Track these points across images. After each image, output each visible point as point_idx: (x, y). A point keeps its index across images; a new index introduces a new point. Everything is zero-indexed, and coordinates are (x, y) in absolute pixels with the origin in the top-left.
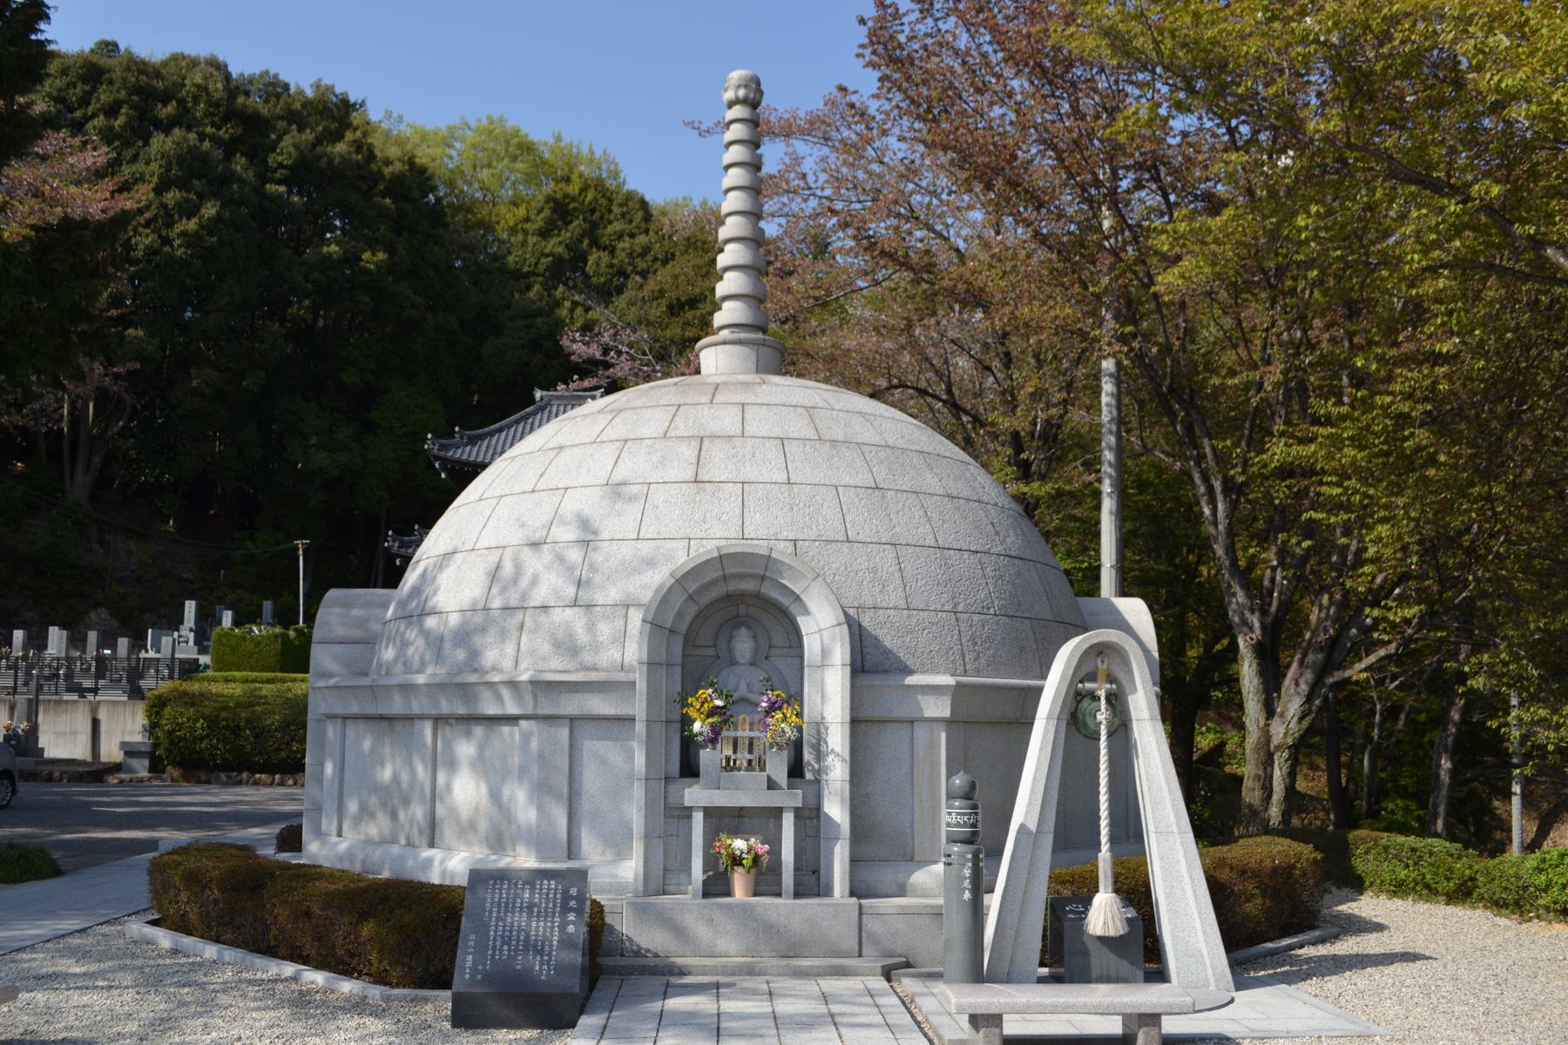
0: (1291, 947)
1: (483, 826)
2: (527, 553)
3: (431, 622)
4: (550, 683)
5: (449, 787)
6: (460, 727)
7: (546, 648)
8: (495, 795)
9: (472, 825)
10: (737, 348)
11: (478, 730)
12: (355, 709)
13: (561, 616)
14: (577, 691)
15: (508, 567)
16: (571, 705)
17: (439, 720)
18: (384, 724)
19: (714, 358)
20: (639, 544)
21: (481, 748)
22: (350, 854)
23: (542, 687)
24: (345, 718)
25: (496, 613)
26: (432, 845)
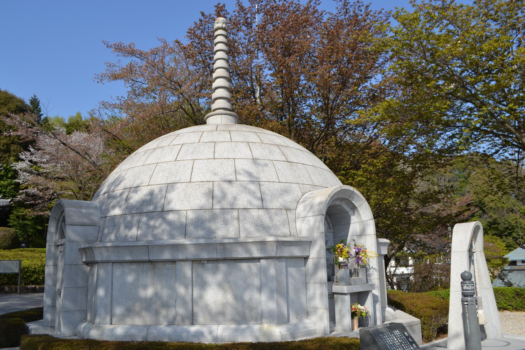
0: (28, 305)
1: (229, 312)
2: (226, 186)
3: (171, 217)
4: (283, 242)
5: (201, 297)
6: (210, 265)
7: (252, 229)
8: (238, 298)
9: (222, 313)
10: (230, 117)
11: (223, 267)
12: (128, 258)
13: (255, 213)
14: (291, 246)
15: (217, 192)
16: (287, 252)
17: (197, 262)
18: (147, 266)
19: (213, 120)
20: (149, 187)
21: (227, 275)
22: (126, 335)
23: (281, 244)
24: (113, 262)
25: (218, 211)
26: (192, 324)
